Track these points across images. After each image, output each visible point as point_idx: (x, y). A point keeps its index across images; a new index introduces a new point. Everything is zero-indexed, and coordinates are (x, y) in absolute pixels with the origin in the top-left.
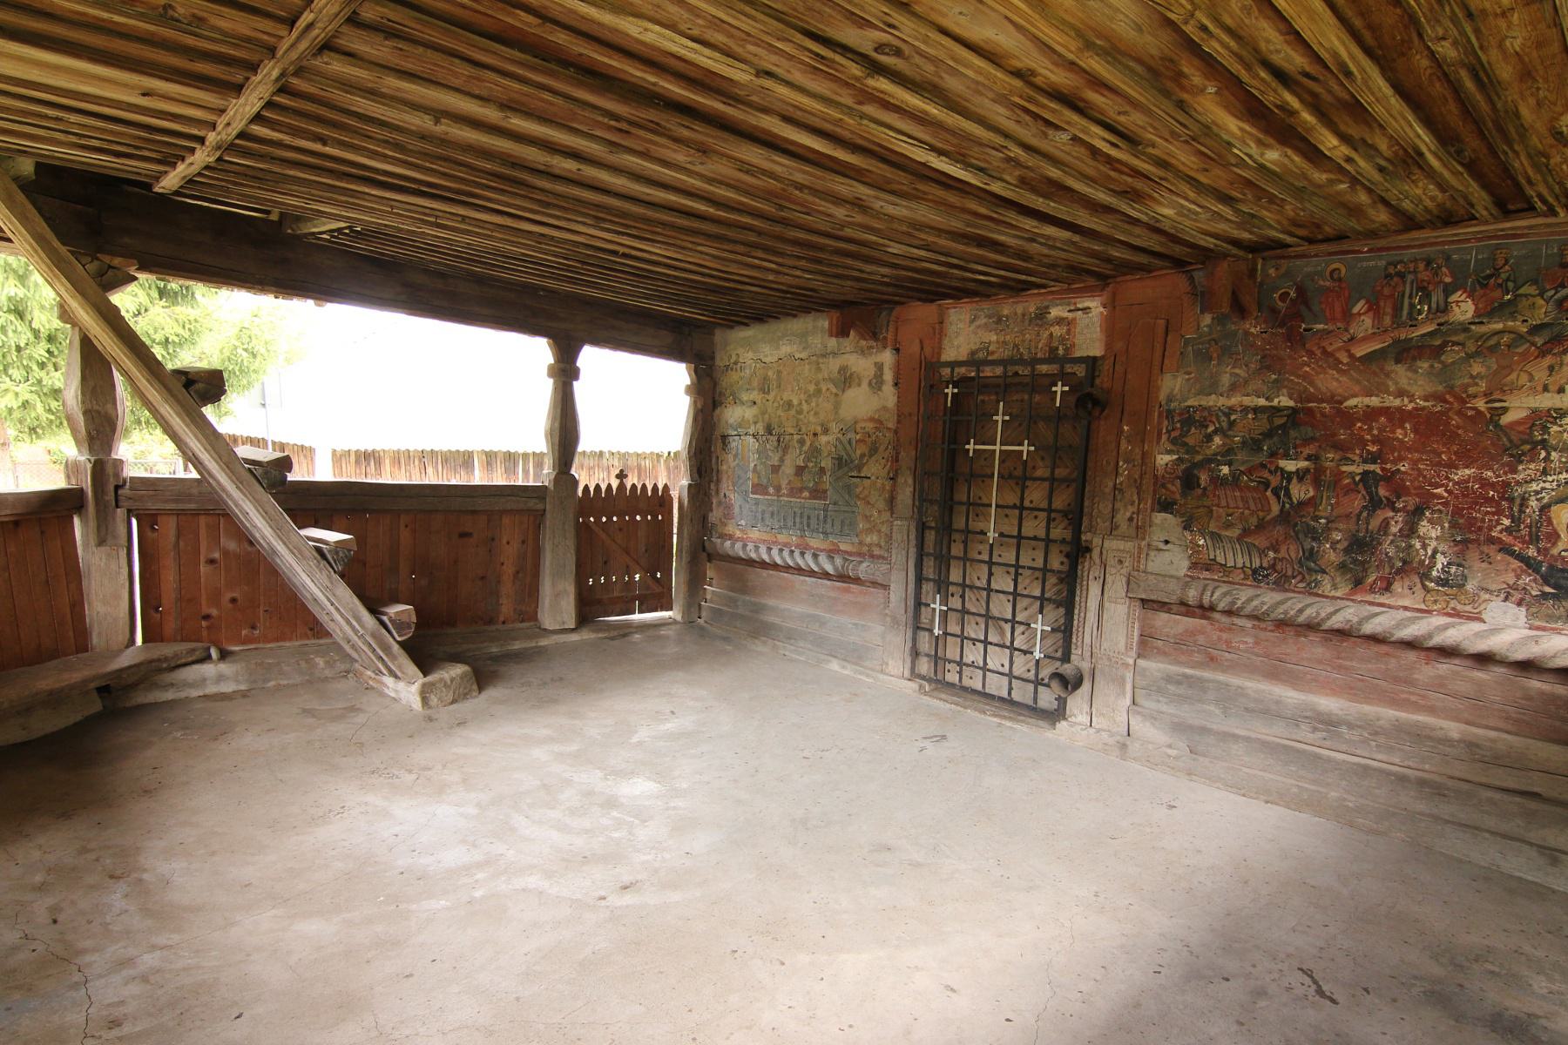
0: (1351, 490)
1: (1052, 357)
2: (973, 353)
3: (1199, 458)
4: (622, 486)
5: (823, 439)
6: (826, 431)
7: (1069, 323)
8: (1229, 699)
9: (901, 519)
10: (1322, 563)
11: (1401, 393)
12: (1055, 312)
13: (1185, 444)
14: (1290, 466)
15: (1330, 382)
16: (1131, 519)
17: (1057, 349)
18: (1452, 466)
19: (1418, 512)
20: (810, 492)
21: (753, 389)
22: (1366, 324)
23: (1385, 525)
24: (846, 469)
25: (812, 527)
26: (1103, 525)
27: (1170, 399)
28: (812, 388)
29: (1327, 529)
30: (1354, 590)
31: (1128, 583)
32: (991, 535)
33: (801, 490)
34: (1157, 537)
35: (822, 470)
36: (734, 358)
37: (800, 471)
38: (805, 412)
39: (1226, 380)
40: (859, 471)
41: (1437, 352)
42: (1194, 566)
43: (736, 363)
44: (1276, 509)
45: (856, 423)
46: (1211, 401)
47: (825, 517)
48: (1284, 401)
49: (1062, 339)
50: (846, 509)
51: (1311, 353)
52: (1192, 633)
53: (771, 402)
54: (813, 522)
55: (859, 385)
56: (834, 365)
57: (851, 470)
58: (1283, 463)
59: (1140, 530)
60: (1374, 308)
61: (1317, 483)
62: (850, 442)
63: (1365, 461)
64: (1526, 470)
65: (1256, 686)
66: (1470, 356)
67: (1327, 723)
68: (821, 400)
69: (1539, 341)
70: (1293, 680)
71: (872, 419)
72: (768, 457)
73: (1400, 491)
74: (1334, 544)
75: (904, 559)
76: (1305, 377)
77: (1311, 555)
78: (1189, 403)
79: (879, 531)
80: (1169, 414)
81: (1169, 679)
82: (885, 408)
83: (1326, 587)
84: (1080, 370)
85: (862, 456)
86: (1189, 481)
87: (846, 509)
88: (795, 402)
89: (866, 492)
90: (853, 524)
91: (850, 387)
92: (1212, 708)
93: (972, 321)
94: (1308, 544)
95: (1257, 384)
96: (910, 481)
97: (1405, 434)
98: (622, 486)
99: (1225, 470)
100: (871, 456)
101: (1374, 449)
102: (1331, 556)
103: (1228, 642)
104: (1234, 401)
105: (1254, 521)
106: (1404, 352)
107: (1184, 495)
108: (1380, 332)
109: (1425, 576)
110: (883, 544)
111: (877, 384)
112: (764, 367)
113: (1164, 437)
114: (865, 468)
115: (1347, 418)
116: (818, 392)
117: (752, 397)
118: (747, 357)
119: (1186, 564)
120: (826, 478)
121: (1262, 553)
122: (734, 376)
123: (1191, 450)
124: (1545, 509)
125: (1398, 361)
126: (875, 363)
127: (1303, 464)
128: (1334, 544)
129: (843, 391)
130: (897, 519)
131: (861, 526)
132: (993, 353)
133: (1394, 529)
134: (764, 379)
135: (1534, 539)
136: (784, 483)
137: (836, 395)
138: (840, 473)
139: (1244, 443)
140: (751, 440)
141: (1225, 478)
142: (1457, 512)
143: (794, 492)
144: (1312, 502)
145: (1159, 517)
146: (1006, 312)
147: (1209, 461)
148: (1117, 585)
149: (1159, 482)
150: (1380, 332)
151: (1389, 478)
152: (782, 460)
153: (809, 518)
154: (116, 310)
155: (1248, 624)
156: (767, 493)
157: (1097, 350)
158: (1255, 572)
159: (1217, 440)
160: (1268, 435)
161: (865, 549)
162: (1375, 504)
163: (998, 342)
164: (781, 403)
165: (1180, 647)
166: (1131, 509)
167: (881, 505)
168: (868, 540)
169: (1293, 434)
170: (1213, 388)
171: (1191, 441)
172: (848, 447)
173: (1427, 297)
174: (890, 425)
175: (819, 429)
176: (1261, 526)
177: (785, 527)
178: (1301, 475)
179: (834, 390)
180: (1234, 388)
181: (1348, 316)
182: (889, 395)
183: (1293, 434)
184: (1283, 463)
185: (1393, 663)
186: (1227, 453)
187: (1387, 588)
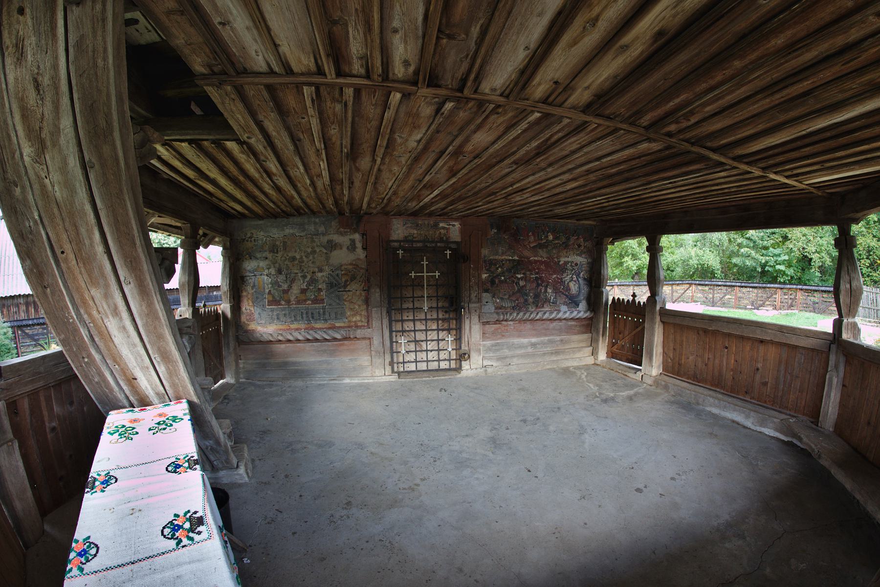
0: (533, 282)
1: (441, 240)
2: (406, 237)
3: (495, 275)
4: (634, 300)
5: (320, 275)
6: (321, 270)
7: (448, 229)
8: (511, 347)
9: (376, 307)
10: (529, 302)
11: (541, 257)
12: (441, 225)
13: (490, 271)
14: (519, 276)
15: (526, 253)
16: (476, 296)
17: (443, 238)
18: (552, 275)
19: (546, 287)
20: (312, 301)
21: (265, 251)
23: (541, 290)
24: (336, 288)
25: (315, 318)
26: (467, 299)
27: (485, 257)
28: (309, 250)
29: (529, 293)
30: (536, 309)
31: (479, 317)
33: (305, 300)
34: (484, 302)
35: (320, 290)
36: (249, 235)
37: (303, 291)
38: (305, 262)
39: (500, 251)
40: (345, 288)
41: (547, 247)
42: (496, 308)
43: (251, 237)
44: (516, 289)
45: (341, 266)
46: (497, 257)
47: (324, 312)
48: (516, 258)
49: (445, 235)
50: (338, 307)
51: (521, 245)
52: (497, 329)
53: (279, 258)
54: (316, 316)
55: (341, 249)
56: (325, 239)
57: (340, 288)
58: (517, 275)
59: (479, 300)
60: (533, 234)
61: (526, 281)
62: (337, 275)
63: (536, 274)
64: (565, 275)
65: (516, 341)
66: (553, 248)
67: (534, 345)
68: (316, 256)
69: (564, 246)
70: (524, 337)
71: (351, 264)
72: (279, 286)
73: (543, 282)
74: (531, 297)
75: (380, 325)
76: (520, 251)
77: (526, 300)
78: (491, 258)
79: (361, 315)
80: (485, 261)
81: (492, 346)
82: (359, 259)
83: (530, 309)
84: (453, 246)
85: (346, 281)
86: (493, 282)
87: (338, 307)
88: (298, 257)
89: (350, 298)
90: (343, 314)
91: (335, 249)
92: (506, 350)
93: (404, 225)
94: (526, 297)
96: (378, 290)
97: (543, 267)
98: (634, 300)
99: (503, 278)
100: (352, 281)
101: (537, 271)
102: (531, 300)
103: (507, 330)
104: (503, 257)
105: (511, 293)
106: (541, 246)
107: (492, 286)
108: (535, 241)
109: (550, 302)
110: (363, 320)
111: (352, 247)
112: (272, 240)
113: (484, 269)
114: (349, 287)
115: (531, 262)
116: (314, 252)
117: (264, 255)
118: (261, 235)
119: (494, 308)
121: (514, 301)
123: (492, 273)
124: (568, 283)
125: (540, 248)
126: (350, 239)
127: (522, 275)
128: (531, 297)
129: (331, 252)
130: (373, 308)
131: (349, 314)
132: (415, 238)
133: (543, 291)
134: (274, 246)
135: (567, 291)
136: (292, 298)
137: (326, 253)
138: (332, 290)
139: (507, 269)
140: (266, 278)
141: (502, 281)
142: (554, 286)
143: (298, 302)
144: (525, 286)
145: (484, 295)
146: (420, 223)
147: (498, 275)
148: (475, 319)
150: (535, 241)
151: (541, 278)
152: (290, 287)
153: (312, 314)
154: (28, 274)
155: (511, 323)
156: (280, 305)
157: (458, 239)
158: (513, 307)
159: (500, 269)
161: (353, 324)
162: (538, 285)
163: (417, 233)
164: (288, 257)
165: (494, 333)
166: (476, 293)
167: (360, 303)
168: (354, 319)
169: (519, 267)
170: (497, 254)
171: (492, 270)
172: (337, 278)
173: (544, 234)
174: (363, 267)
176: (514, 294)
177: (296, 320)
178: (522, 278)
179: (325, 251)
180: (503, 254)
181: (528, 236)
182: (361, 253)
183: (519, 267)
184: (517, 275)
185: (545, 326)
186: (503, 274)
187: (543, 307)
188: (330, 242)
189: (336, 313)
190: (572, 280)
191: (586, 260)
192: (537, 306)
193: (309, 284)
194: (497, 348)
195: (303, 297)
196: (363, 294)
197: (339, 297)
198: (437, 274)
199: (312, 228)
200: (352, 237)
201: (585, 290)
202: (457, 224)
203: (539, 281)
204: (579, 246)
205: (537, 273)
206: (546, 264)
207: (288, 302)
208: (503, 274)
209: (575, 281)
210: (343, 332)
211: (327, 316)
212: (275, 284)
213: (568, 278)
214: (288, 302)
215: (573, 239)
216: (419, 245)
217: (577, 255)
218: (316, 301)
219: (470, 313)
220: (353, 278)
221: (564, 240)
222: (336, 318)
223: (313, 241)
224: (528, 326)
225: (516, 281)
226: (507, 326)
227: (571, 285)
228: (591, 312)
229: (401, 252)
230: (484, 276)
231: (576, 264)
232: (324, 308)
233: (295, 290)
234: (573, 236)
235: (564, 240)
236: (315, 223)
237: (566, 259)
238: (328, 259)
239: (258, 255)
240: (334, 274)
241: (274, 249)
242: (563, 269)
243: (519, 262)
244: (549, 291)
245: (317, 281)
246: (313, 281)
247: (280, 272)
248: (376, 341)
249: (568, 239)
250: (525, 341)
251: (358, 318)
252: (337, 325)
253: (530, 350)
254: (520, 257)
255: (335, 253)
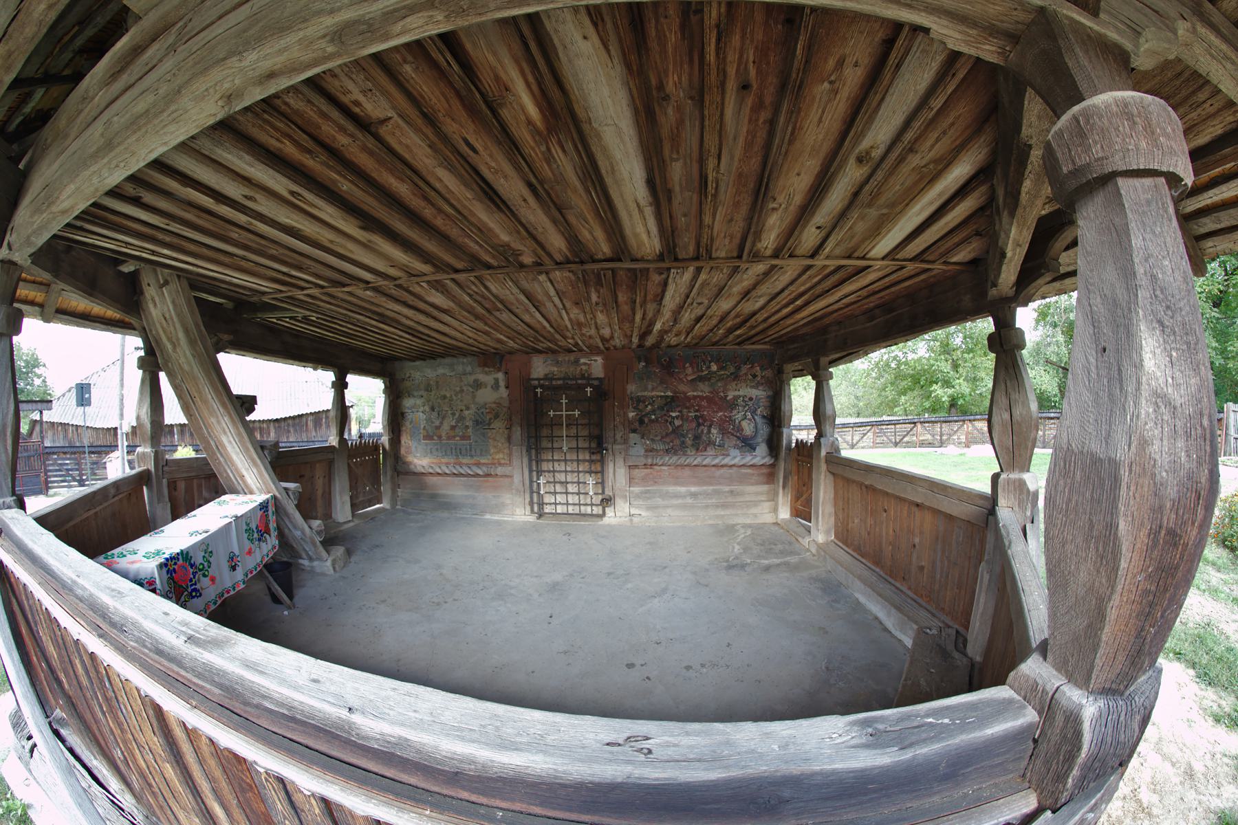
0: (692, 421)
1: (583, 377)
2: (546, 375)
5: (467, 412)
6: (468, 408)
7: (589, 365)
12: (582, 361)
14: (674, 414)
15: (682, 388)
19: (710, 426)
22: (689, 371)
23: (702, 431)
26: (611, 440)
28: (458, 389)
32: (565, 449)
33: (454, 437)
34: (632, 442)
35: (467, 427)
36: (408, 375)
39: (650, 387)
41: (709, 379)
42: (646, 451)
46: (645, 394)
48: (669, 394)
49: (586, 371)
52: (647, 475)
54: (463, 452)
59: (626, 441)
61: (682, 419)
64: (735, 412)
67: (694, 495)
70: (682, 485)
71: (495, 403)
72: (432, 422)
73: (705, 420)
77: (683, 443)
80: (632, 399)
81: (642, 493)
83: (689, 452)
84: (596, 383)
85: (490, 419)
86: (641, 422)
95: (660, 388)
96: (519, 429)
97: (704, 403)
115: (689, 399)
116: (462, 391)
120: (470, 430)
122: (408, 384)
123: (641, 411)
136: (444, 434)
143: (449, 438)
144: (681, 426)
145: (632, 435)
149: (630, 422)
151: (702, 416)
152: (441, 423)
157: (601, 375)
159: (649, 407)
160: (666, 405)
162: (699, 425)
170: (646, 389)
175: (464, 408)
176: (667, 435)
178: (677, 417)
179: (471, 390)
180: (653, 389)
181: (685, 368)
182: (503, 392)
186: (653, 412)
188: (476, 381)
189: (481, 450)
190: (745, 417)
191: (764, 393)
192: (697, 449)
193: (458, 422)
194: (647, 495)
195: (452, 433)
196: (506, 432)
197: (484, 435)
198: (577, 413)
199: (460, 368)
200: (496, 376)
201: (764, 430)
202: (599, 360)
203: (700, 420)
204: (754, 376)
205: (697, 411)
206: (710, 400)
207: (440, 437)
208: (653, 412)
209: (750, 420)
210: (485, 469)
211: (473, 453)
212: (429, 420)
213: (740, 416)
214: (440, 437)
215: (744, 369)
216: (560, 382)
217: (752, 387)
218: (463, 438)
219: (614, 455)
220: (497, 416)
221: (732, 370)
222: (481, 455)
223: (462, 381)
224: (687, 472)
225: (669, 420)
226: (660, 471)
227: (745, 424)
228: (772, 457)
229: (539, 390)
230: (631, 415)
231: (751, 399)
232: (470, 445)
233: (446, 427)
234: (745, 364)
235: (732, 370)
236: (463, 363)
237: (737, 393)
238: (474, 397)
239: (416, 394)
240: (480, 412)
241: (428, 389)
242: (732, 405)
243: (673, 399)
244: (714, 431)
245: (464, 418)
246: (461, 418)
247: (433, 409)
248: (517, 479)
249: (738, 368)
250: (683, 489)
251: (501, 456)
252: (483, 461)
253: (689, 501)
254: (675, 392)
255: (480, 392)
